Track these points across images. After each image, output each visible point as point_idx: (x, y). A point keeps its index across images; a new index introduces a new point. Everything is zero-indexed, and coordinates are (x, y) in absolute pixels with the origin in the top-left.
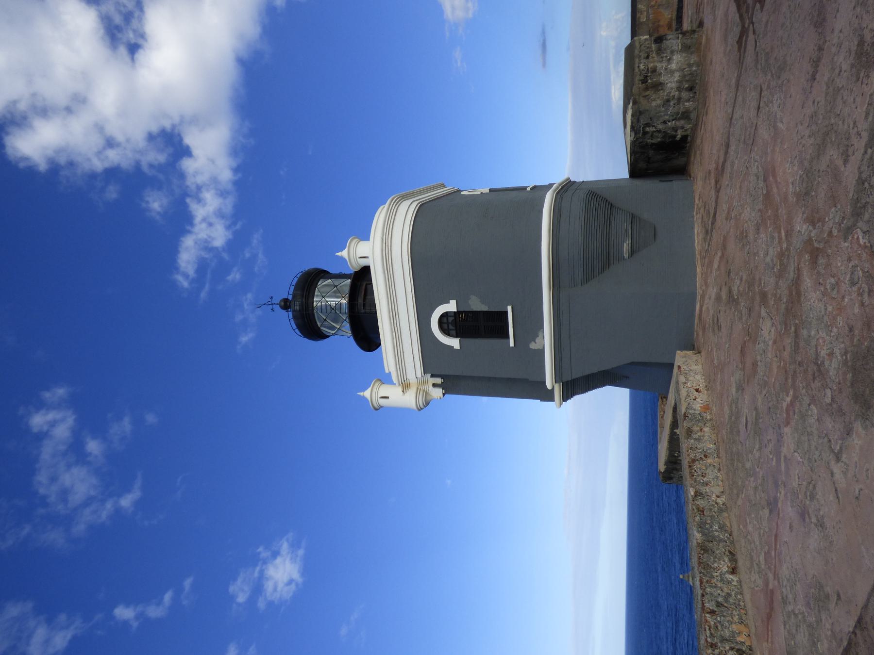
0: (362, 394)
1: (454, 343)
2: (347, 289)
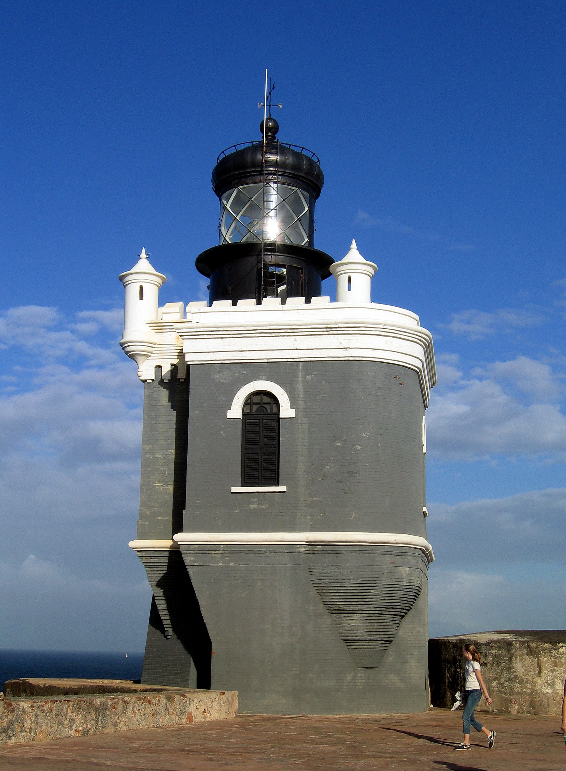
0: (143, 255)
1: (236, 412)
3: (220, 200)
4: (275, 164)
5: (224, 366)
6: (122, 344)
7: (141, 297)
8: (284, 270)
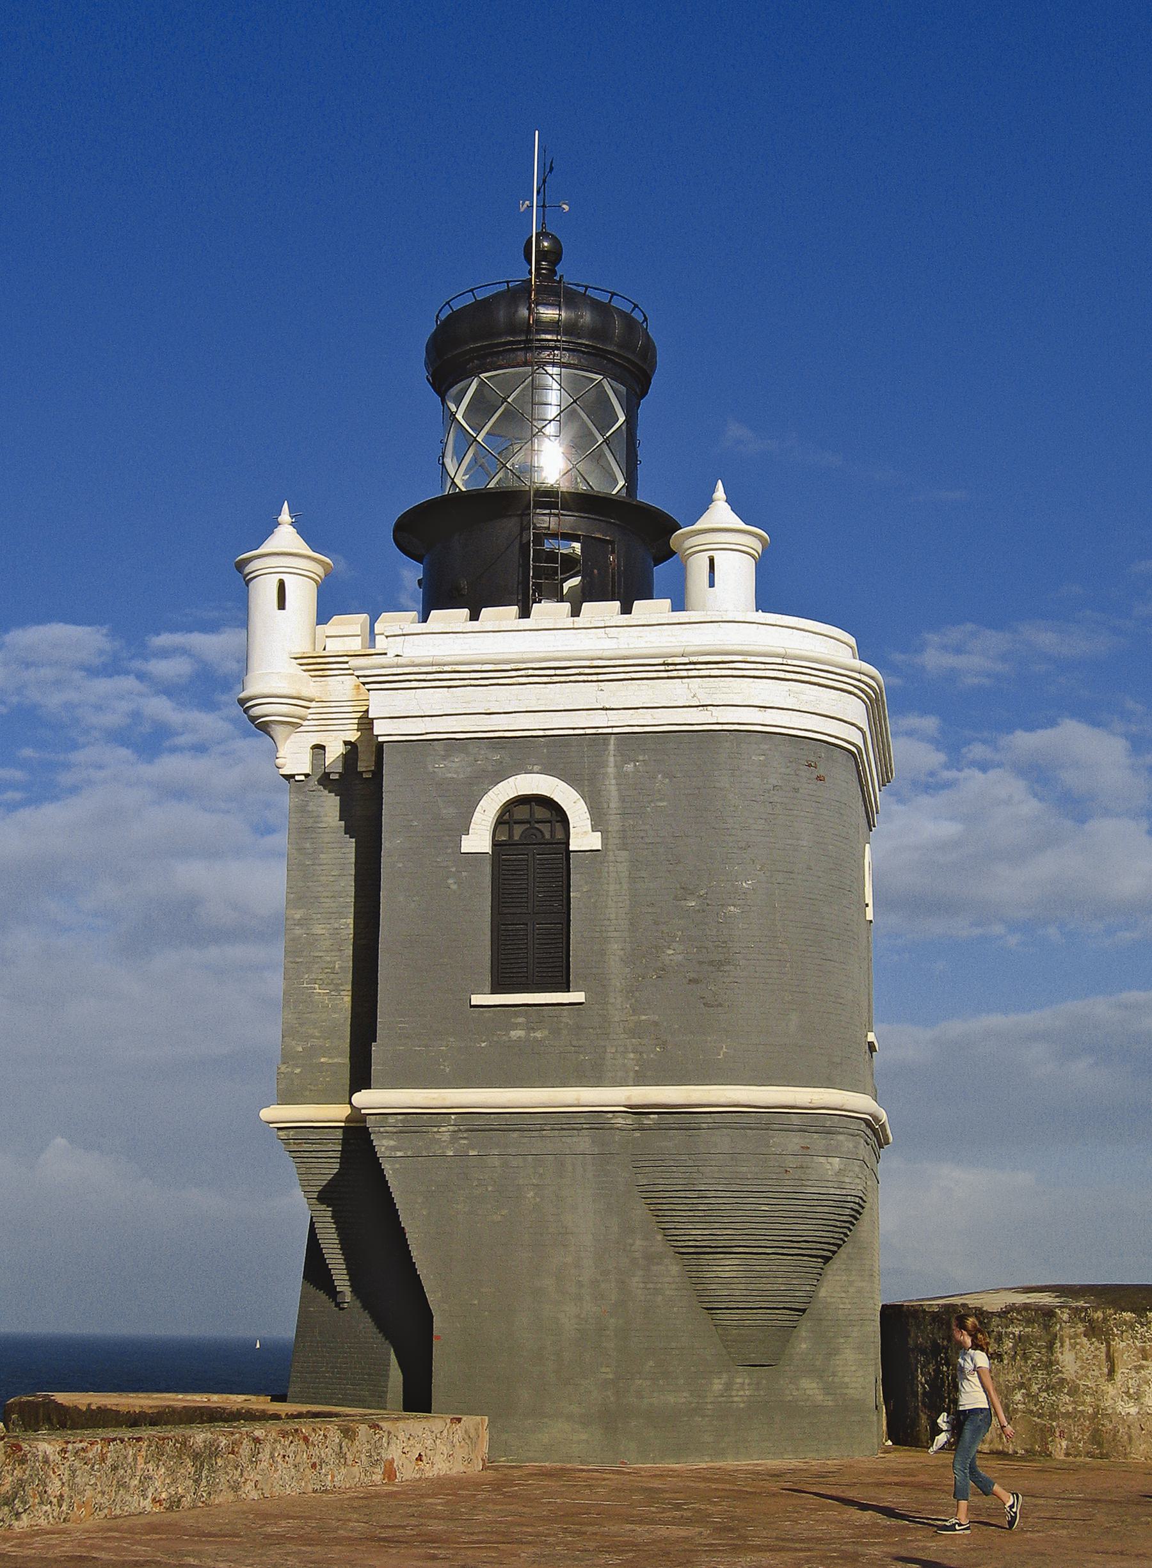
0: (285, 516)
1: (478, 839)
2: (597, 485)
3: (443, 402)
5: (454, 745)
6: (242, 702)
7: (282, 605)
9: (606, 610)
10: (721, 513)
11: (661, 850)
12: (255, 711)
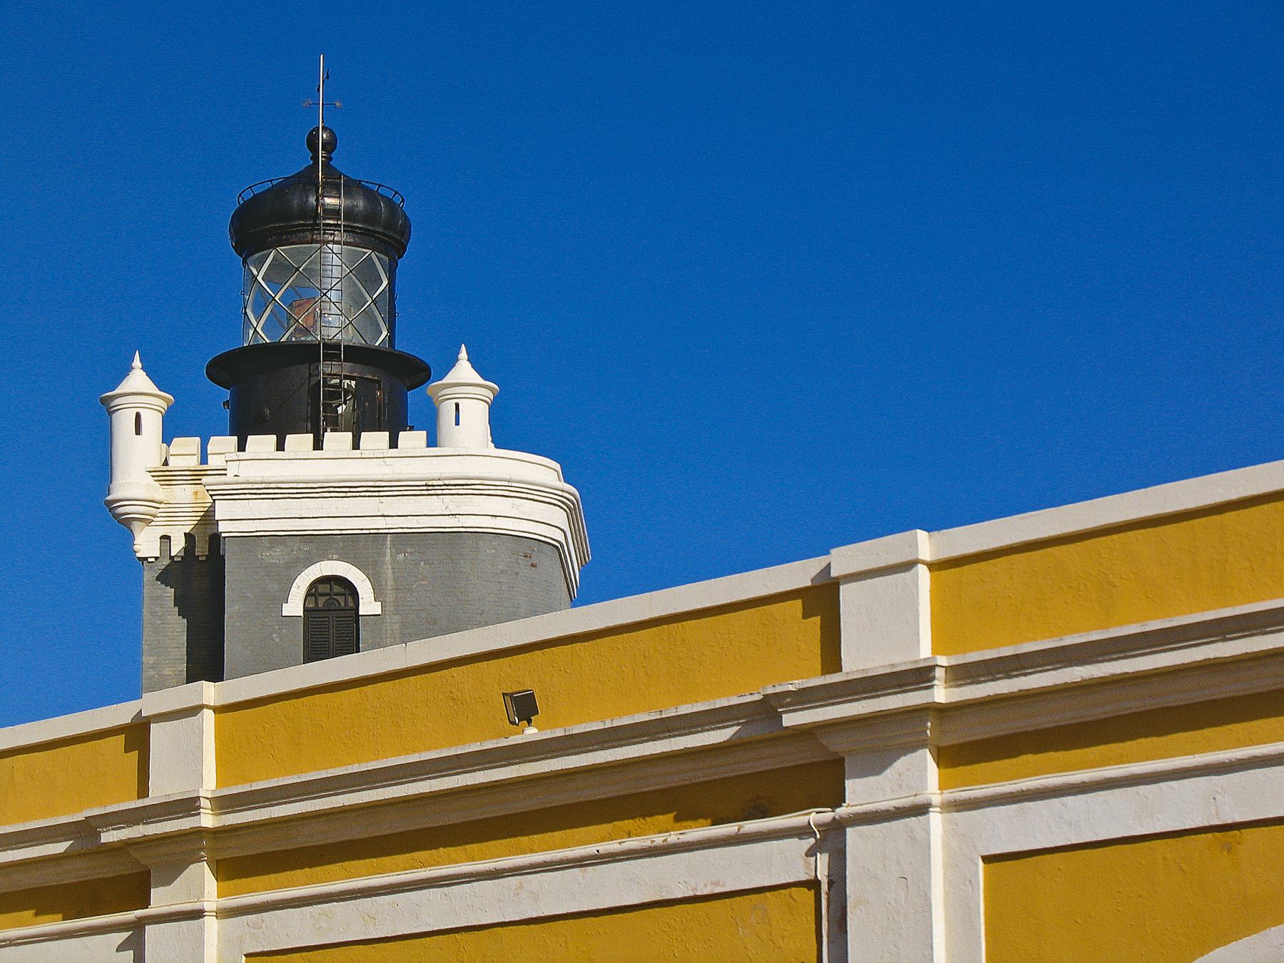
1: (294, 606)
3: (245, 262)
4: (334, 213)
5: (276, 539)
6: (109, 503)
7: (138, 432)
8: (353, 383)
9: (375, 440)
10: (464, 370)
11: (423, 614)
12: (121, 510)
